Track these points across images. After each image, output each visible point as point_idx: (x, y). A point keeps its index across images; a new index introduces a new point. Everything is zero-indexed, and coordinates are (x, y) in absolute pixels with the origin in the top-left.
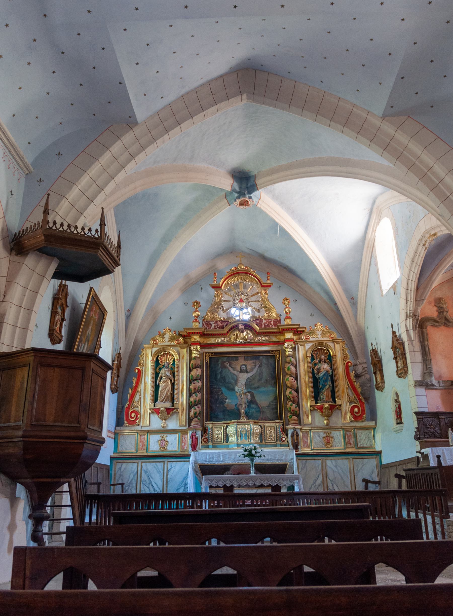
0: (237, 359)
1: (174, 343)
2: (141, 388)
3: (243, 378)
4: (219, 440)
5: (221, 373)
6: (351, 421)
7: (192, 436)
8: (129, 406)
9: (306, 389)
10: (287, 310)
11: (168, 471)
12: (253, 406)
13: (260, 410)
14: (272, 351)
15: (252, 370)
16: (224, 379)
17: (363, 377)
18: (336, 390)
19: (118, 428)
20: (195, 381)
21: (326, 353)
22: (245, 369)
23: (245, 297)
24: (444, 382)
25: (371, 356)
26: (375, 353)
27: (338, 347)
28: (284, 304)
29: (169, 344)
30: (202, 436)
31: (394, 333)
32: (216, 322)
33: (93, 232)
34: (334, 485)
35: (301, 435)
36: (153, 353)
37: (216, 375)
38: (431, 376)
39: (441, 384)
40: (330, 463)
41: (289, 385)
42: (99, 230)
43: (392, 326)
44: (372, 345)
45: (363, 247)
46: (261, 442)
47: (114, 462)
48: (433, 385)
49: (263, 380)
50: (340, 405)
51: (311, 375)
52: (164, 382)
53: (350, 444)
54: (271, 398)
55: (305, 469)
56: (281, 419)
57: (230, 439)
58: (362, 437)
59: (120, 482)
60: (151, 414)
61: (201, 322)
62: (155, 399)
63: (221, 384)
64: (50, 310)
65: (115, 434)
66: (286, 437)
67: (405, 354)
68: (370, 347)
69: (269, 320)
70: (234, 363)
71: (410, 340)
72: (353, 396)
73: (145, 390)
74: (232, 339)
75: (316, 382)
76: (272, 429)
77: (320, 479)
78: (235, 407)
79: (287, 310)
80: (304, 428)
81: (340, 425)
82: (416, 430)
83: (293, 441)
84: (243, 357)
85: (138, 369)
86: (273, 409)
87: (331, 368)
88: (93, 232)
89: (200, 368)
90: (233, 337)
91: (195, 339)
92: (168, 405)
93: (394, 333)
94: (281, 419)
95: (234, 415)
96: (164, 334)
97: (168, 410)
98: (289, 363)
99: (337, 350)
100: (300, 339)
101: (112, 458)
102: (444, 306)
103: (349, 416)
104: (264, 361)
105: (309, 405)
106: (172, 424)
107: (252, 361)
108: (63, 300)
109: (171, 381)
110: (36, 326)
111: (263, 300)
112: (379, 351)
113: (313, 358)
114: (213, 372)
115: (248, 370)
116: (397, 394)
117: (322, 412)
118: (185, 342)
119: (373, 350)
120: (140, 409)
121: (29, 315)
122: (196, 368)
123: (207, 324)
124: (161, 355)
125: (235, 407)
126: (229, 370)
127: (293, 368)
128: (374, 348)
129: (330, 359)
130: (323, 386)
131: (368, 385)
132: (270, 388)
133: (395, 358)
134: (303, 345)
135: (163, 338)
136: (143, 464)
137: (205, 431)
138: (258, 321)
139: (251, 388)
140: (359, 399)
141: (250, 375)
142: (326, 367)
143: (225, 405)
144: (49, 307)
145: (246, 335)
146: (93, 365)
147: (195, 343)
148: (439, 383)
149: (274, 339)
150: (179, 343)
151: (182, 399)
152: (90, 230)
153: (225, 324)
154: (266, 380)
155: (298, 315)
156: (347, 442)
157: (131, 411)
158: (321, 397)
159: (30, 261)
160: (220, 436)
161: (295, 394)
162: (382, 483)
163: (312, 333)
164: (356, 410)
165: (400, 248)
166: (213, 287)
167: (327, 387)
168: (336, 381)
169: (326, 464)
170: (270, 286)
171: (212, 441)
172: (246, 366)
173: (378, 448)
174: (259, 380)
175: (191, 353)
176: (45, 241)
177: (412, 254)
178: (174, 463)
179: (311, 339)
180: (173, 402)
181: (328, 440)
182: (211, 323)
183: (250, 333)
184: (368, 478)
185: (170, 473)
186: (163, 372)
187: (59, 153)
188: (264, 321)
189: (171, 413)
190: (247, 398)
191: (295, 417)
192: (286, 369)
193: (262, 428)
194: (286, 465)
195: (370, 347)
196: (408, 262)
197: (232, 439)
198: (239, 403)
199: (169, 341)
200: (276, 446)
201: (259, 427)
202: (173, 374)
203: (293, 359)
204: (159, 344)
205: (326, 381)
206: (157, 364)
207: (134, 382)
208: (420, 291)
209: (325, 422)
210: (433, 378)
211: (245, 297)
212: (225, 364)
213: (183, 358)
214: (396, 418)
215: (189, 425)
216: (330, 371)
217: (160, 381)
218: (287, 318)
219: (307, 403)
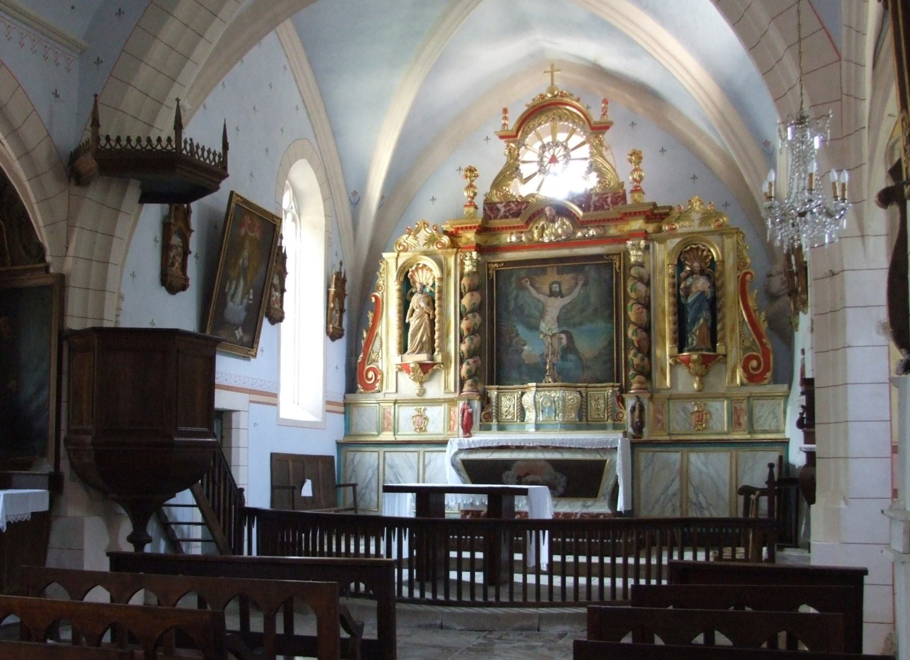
0: (544, 271)
2: (381, 329)
3: (554, 306)
4: (509, 417)
5: (517, 297)
6: (742, 384)
8: (364, 359)
11: (424, 467)
12: (571, 357)
13: (583, 365)
14: (608, 255)
16: (520, 308)
19: (351, 396)
22: (558, 290)
23: (562, 152)
32: (508, 203)
34: (700, 495)
40: (696, 459)
42: (173, 138)
46: (580, 420)
47: (343, 450)
53: (740, 424)
54: (600, 343)
57: (527, 413)
58: (762, 410)
59: (353, 482)
60: (399, 374)
61: (480, 205)
62: (403, 349)
63: (515, 318)
64: (159, 245)
65: (345, 405)
73: (387, 332)
74: (536, 235)
75: (680, 310)
77: (676, 485)
81: (722, 391)
82: (801, 410)
84: (555, 268)
85: (376, 298)
87: (713, 286)
91: (468, 239)
92: (423, 357)
100: (659, 230)
101: (340, 445)
104: (593, 274)
105: (668, 353)
108: (180, 224)
109: (429, 315)
110: (133, 275)
113: (680, 266)
114: (495, 301)
117: (689, 368)
120: (382, 365)
121: (106, 270)
123: (491, 209)
124: (413, 271)
126: (530, 292)
129: (710, 269)
130: (700, 323)
132: (601, 325)
134: (662, 241)
136: (387, 455)
137: (485, 400)
141: (567, 300)
142: (701, 284)
144: (155, 240)
153: (523, 207)
154: (596, 310)
156: (734, 422)
157: (367, 367)
158: (690, 340)
160: (511, 409)
161: (644, 334)
163: (683, 215)
164: (754, 363)
168: (720, 310)
169: (688, 459)
171: (497, 418)
172: (559, 284)
174: (583, 310)
181: (702, 418)
182: (499, 206)
183: (567, 223)
186: (417, 301)
187: (120, 10)
189: (430, 371)
193: (582, 397)
197: (530, 416)
200: (603, 428)
205: (699, 310)
206: (407, 286)
207: (371, 319)
209: (695, 386)
213: (449, 274)
215: (461, 391)
217: (411, 316)
219: (665, 351)
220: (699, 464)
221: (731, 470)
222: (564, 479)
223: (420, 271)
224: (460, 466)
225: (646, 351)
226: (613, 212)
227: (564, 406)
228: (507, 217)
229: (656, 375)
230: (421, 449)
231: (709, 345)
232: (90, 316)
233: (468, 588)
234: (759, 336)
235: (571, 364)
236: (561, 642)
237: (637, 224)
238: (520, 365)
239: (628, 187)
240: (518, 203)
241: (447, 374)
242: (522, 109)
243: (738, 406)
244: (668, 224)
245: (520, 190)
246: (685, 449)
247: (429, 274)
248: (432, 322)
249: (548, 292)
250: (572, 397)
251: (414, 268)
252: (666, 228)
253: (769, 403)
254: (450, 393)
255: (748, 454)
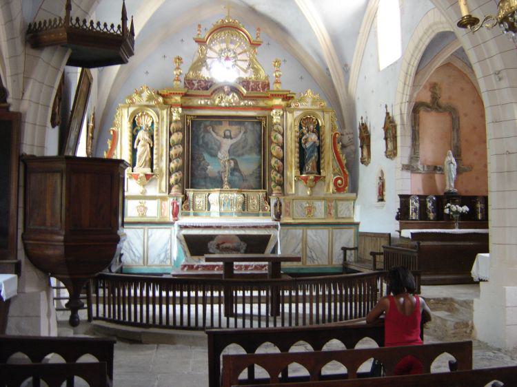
0: (221, 123)
1: (153, 103)
3: (227, 144)
5: (203, 137)
7: (173, 204)
9: (293, 158)
10: (277, 74)
12: (236, 173)
13: (244, 179)
15: (236, 136)
17: (349, 148)
18: (322, 161)
20: (176, 146)
21: (315, 123)
23: (232, 55)
24: (428, 166)
25: (360, 129)
26: (364, 128)
27: (327, 116)
28: (275, 66)
29: (147, 103)
30: (183, 203)
31: (388, 114)
32: (199, 81)
33: (116, 28)
35: (283, 204)
36: (130, 114)
37: (198, 140)
38: (417, 161)
39: (425, 169)
40: (311, 233)
41: (275, 154)
43: (386, 107)
44: (362, 118)
45: (364, 18)
46: (244, 210)
48: (418, 169)
49: (248, 147)
50: (325, 177)
51: (298, 145)
52: (143, 146)
53: (331, 214)
55: (286, 238)
56: (264, 188)
58: (342, 206)
61: (183, 80)
66: (268, 206)
67: (396, 137)
68: (359, 121)
69: (257, 83)
70: (218, 128)
71: (403, 124)
72: (338, 169)
74: (217, 102)
75: (302, 152)
76: (256, 197)
77: (300, 246)
78: (217, 174)
79: (277, 74)
80: (287, 198)
81: (323, 196)
83: (275, 211)
84: (228, 122)
85: (114, 132)
86: (256, 178)
87: (319, 138)
88: (116, 28)
89: (180, 131)
90: (218, 99)
91: (176, 100)
93: (388, 114)
94: (264, 188)
95: (217, 183)
96: (142, 92)
97: (147, 176)
98: (276, 131)
99: (325, 121)
100: (288, 106)
102: (438, 92)
103: (332, 187)
104: (250, 127)
106: (152, 190)
107: (237, 127)
111: (251, 60)
112: (368, 125)
113: (301, 127)
115: (232, 136)
116: (382, 172)
118: (165, 103)
119: (363, 124)
122: (177, 131)
123: (189, 83)
125: (217, 174)
127: (280, 137)
128: (364, 122)
129: (318, 130)
130: (309, 158)
131: (353, 156)
133: (386, 139)
134: (291, 112)
135: (140, 96)
137: (186, 198)
138: (246, 83)
139: (235, 156)
140: (343, 170)
141: (234, 141)
142: (314, 137)
143: (208, 171)
145: (233, 98)
146: (122, 165)
147: (176, 105)
148: (424, 167)
149: (261, 104)
150: (159, 103)
151: (162, 164)
152: (112, 26)
154: (251, 147)
155: (284, 77)
156: (328, 213)
158: (307, 168)
159: (45, 54)
161: (280, 163)
162: (359, 249)
164: (339, 181)
165: (406, 30)
166: (196, 41)
167: (314, 158)
168: (322, 153)
170: (260, 45)
173: (356, 220)
174: (243, 148)
175: (171, 115)
176: (68, 39)
177: (417, 40)
178: (155, 230)
179: (300, 107)
180: (152, 166)
181: (310, 210)
182: (194, 82)
183: (236, 96)
184: (345, 246)
185: (151, 239)
186: (142, 135)
188: (251, 84)
189: (150, 179)
190: (230, 165)
191: (278, 187)
192: (273, 138)
194: (270, 236)
195: (359, 121)
196: (412, 46)
198: (222, 170)
199: (147, 101)
200: (258, 215)
201: (242, 196)
202: (152, 137)
203: (280, 128)
204: (137, 103)
205: (313, 152)
206: (134, 126)
207: (110, 145)
208: (419, 77)
209: (308, 193)
210: (419, 163)
211: (232, 55)
212: (208, 128)
213: (163, 119)
214: (378, 194)
216: (318, 142)
217: (138, 144)
218: (277, 82)
219: (292, 173)
220: (312, 235)
221: (329, 237)
222: (246, 245)
223: (143, 117)
224: (183, 238)
225: (282, 172)
226: (261, 93)
227: (236, 202)
228: (199, 89)
229: (286, 186)
230: (146, 227)
231: (316, 172)
232: (36, 144)
233: (102, 299)
234: (342, 167)
235: (236, 178)
236: (440, 364)
237: (278, 102)
238: (206, 177)
239: (271, 81)
240: (206, 82)
241: (161, 181)
242: (210, 27)
243: (330, 204)
244: (295, 103)
245: (205, 73)
246: (305, 228)
247: (149, 119)
248: (152, 149)
249: (223, 135)
250: (240, 197)
251: (140, 114)
252: (293, 105)
253: (345, 203)
254: (163, 192)
255: (338, 230)
